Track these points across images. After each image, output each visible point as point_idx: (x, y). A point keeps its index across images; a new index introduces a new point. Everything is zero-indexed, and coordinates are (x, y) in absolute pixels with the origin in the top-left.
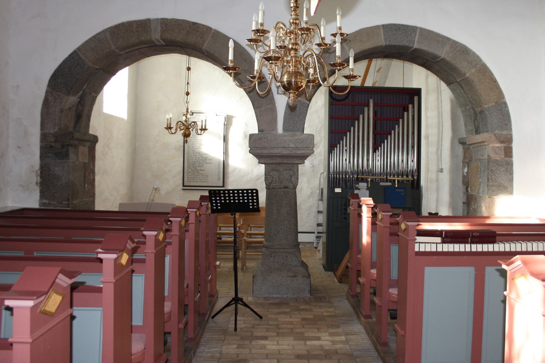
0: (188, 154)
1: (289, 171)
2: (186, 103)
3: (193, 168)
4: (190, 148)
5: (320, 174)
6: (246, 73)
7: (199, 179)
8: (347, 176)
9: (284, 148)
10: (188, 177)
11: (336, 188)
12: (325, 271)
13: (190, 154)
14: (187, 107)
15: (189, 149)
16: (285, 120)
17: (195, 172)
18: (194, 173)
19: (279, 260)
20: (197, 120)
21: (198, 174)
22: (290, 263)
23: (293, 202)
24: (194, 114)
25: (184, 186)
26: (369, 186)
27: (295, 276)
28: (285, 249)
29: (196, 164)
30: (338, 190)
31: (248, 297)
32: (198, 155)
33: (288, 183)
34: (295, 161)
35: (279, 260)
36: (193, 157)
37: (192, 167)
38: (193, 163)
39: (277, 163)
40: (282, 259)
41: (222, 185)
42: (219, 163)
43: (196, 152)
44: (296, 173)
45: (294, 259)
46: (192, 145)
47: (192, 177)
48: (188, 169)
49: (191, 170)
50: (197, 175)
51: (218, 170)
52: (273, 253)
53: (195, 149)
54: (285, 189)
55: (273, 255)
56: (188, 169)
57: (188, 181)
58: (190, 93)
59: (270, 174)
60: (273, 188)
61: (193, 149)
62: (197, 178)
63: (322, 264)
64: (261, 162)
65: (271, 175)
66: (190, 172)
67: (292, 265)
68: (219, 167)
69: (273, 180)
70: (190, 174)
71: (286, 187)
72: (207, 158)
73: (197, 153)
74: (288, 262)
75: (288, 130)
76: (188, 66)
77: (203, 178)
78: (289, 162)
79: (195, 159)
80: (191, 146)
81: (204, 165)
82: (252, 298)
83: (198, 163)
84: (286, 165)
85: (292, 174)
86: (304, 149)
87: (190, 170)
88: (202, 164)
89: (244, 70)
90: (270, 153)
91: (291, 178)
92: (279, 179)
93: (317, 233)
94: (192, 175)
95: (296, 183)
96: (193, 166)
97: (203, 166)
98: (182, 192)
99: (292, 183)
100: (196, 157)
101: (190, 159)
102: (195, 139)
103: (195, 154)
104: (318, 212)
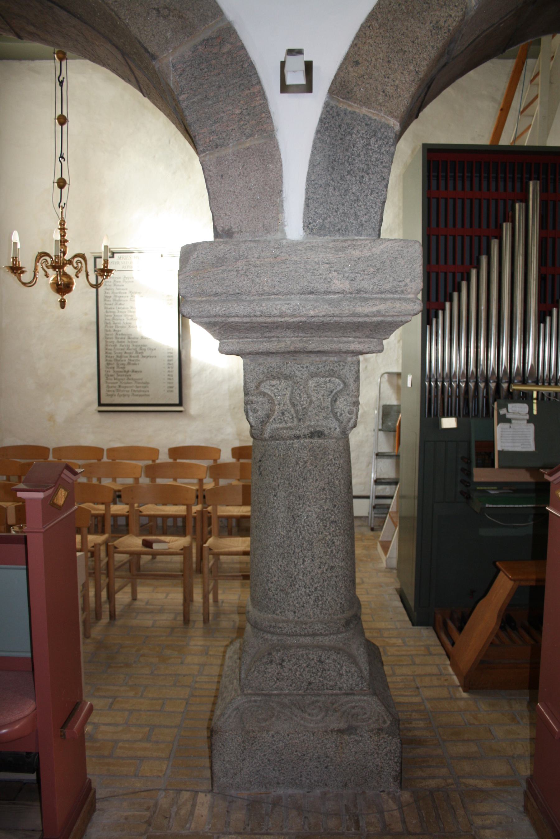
0: (106, 338)
1: (328, 379)
2: (59, 207)
3: (118, 367)
4: (111, 327)
5: (380, 375)
6: (165, 17)
7: (130, 389)
8: (445, 383)
9: (312, 293)
10: (108, 387)
11: (444, 416)
12: (413, 625)
13: (110, 338)
14: (60, 216)
15: (108, 329)
16: (314, 193)
17: (121, 376)
18: (119, 377)
19: (298, 673)
20: (123, 267)
21: (128, 379)
22: (331, 683)
23: (342, 481)
24: (115, 255)
25: (100, 404)
26: (535, 412)
27: (350, 730)
28: (314, 635)
29: (123, 359)
30: (449, 423)
31: (197, 792)
32: (126, 340)
33: (326, 418)
34: (350, 342)
35: (298, 673)
36: (116, 345)
37: (115, 366)
38: (117, 356)
39: (283, 353)
40: (307, 669)
41: (177, 402)
42: (170, 356)
43: (122, 334)
44: (352, 386)
45: (344, 668)
46: (113, 319)
47: (117, 385)
48: (108, 370)
49: (114, 372)
50: (126, 381)
51: (169, 371)
52: (278, 651)
53: (120, 329)
54: (316, 441)
55: (277, 656)
56: (108, 370)
57: (108, 395)
58: (68, 182)
59: (262, 389)
60: (273, 438)
61: (116, 329)
62: (126, 387)
63: (396, 589)
64: (227, 348)
65: (264, 394)
66: (112, 376)
67: (340, 689)
68: (170, 365)
69: (272, 411)
70: (111, 379)
71: (320, 434)
72: (145, 346)
73: (123, 336)
74: (325, 678)
75: (322, 227)
76: (59, 113)
77: (137, 387)
78: (326, 347)
79: (122, 349)
80: (112, 322)
81: (139, 361)
82: (209, 796)
83: (127, 357)
84: (318, 359)
85: (339, 388)
86: (383, 296)
87: (112, 372)
88: (136, 359)
89: (158, 10)
90: (259, 313)
91: (335, 401)
92: (294, 405)
93: (374, 497)
94: (117, 383)
95: (352, 421)
96: (118, 364)
97: (137, 362)
98: (98, 416)
99: (337, 419)
100: (123, 344)
101: (110, 350)
102: (119, 308)
103: (122, 338)
104: (377, 455)
